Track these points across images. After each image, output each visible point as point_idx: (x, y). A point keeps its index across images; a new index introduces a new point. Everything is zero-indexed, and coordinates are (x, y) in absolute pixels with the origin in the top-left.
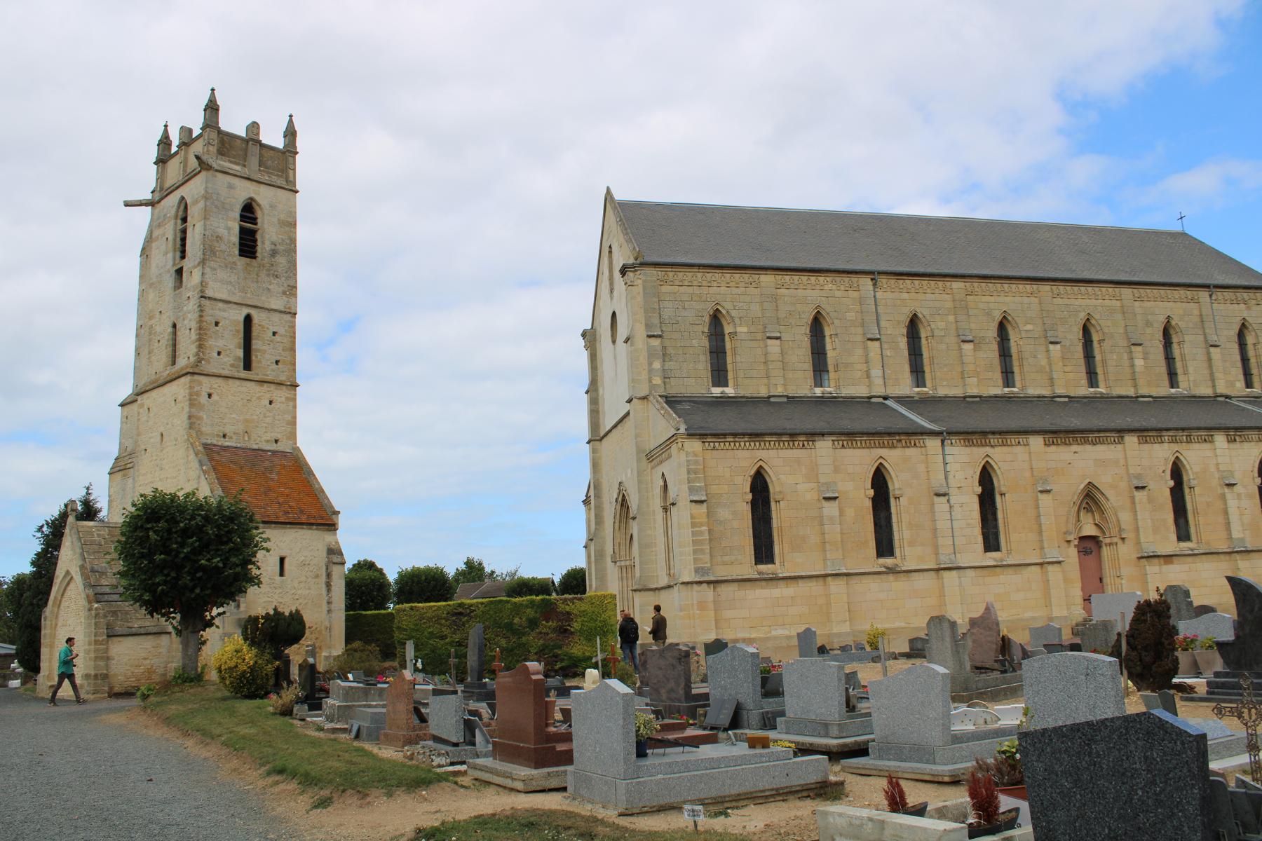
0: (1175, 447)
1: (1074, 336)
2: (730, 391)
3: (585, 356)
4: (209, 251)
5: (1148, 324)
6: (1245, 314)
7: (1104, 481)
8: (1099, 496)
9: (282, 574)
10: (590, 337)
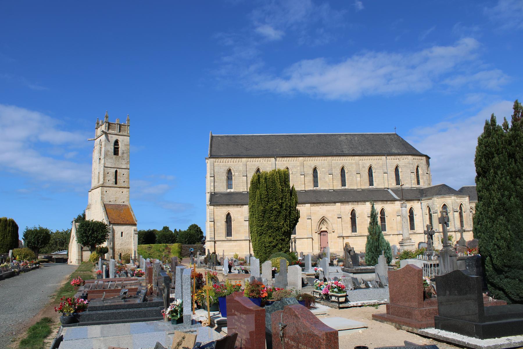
0: (353, 206)
1: (338, 172)
2: (232, 190)
4: (106, 155)
6: (398, 163)
7: (328, 216)
8: (327, 220)
9: (122, 236)
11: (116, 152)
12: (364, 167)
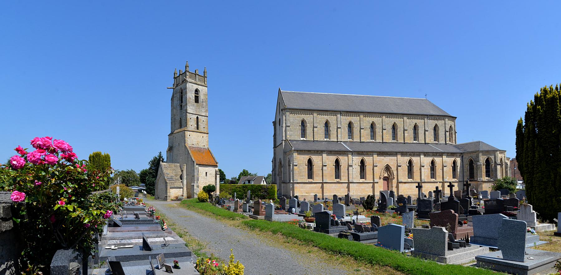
2: (305, 139)
3: (273, 127)
5: (410, 125)
10: (274, 123)
11: (197, 100)
12: (410, 125)
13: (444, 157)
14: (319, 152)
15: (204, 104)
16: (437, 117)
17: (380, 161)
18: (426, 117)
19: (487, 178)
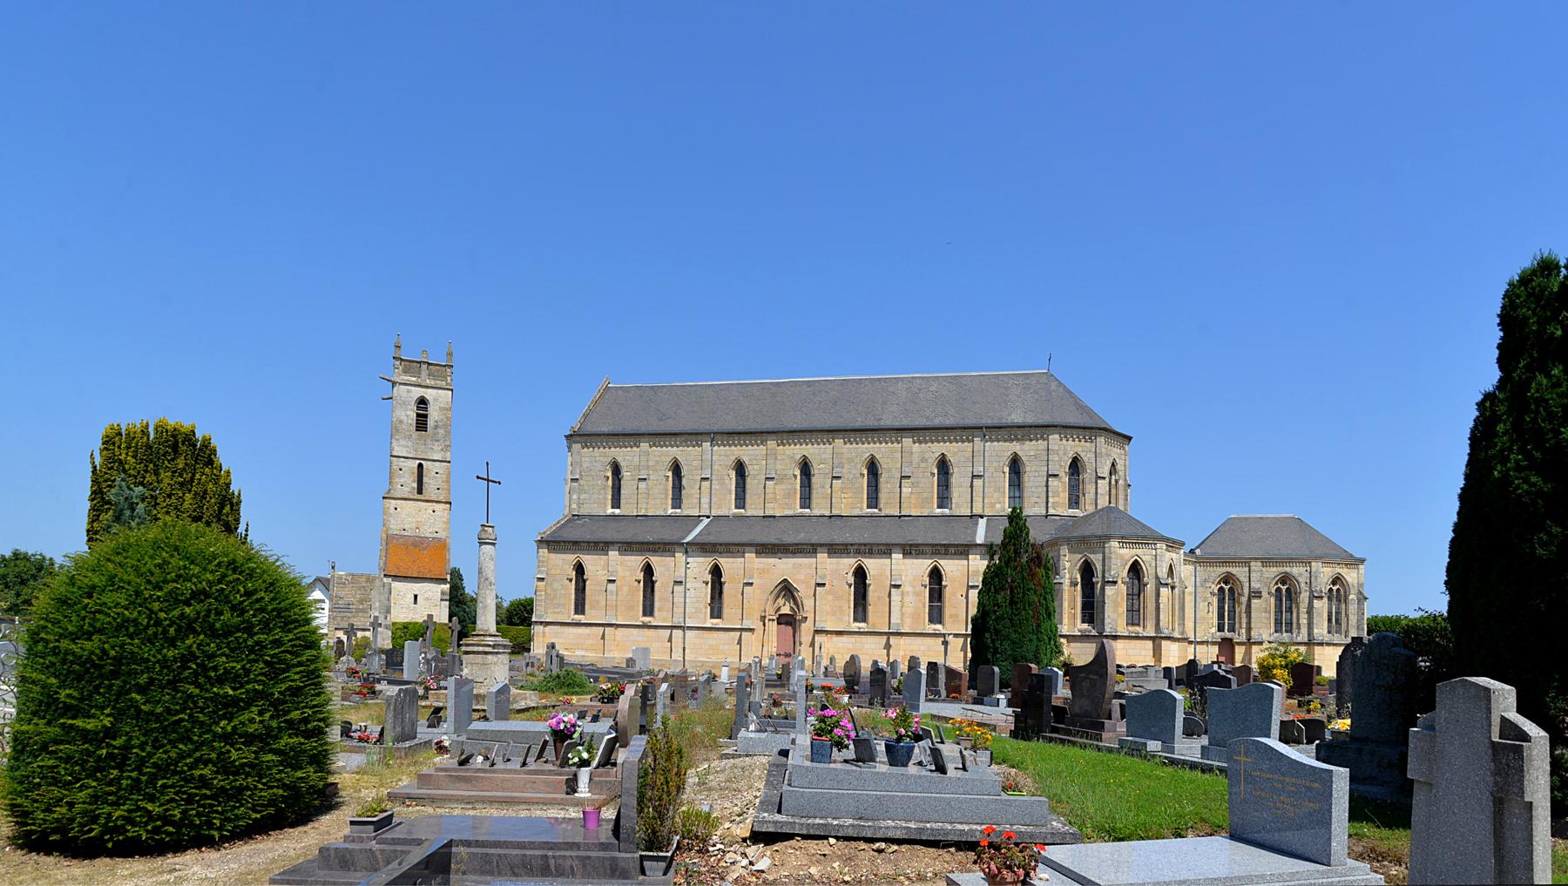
2: (946, 511)
11: (422, 423)
12: (924, 460)
13: (897, 556)
14: (601, 547)
15: (441, 431)
16: (1020, 433)
17: (762, 572)
18: (976, 432)
19: (1085, 626)
